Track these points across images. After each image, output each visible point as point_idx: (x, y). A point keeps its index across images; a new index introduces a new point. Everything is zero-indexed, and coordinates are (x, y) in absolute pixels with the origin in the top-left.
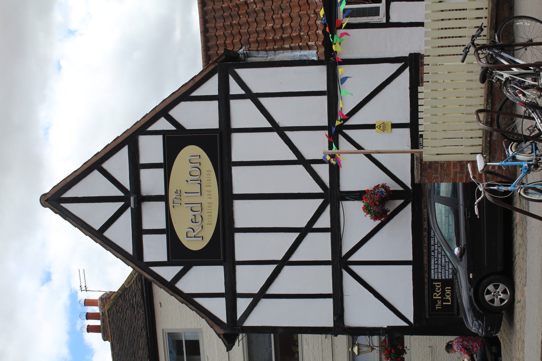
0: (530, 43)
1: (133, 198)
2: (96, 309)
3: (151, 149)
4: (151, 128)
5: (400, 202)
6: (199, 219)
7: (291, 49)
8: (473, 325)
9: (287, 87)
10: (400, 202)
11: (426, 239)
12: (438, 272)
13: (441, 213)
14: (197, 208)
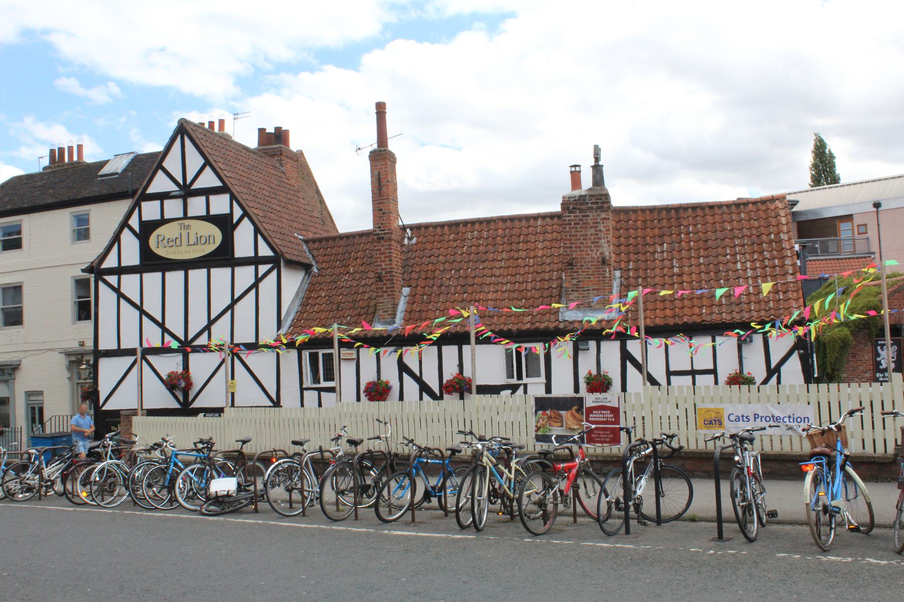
3: (220, 205)
5: (181, 399)
6: (171, 244)
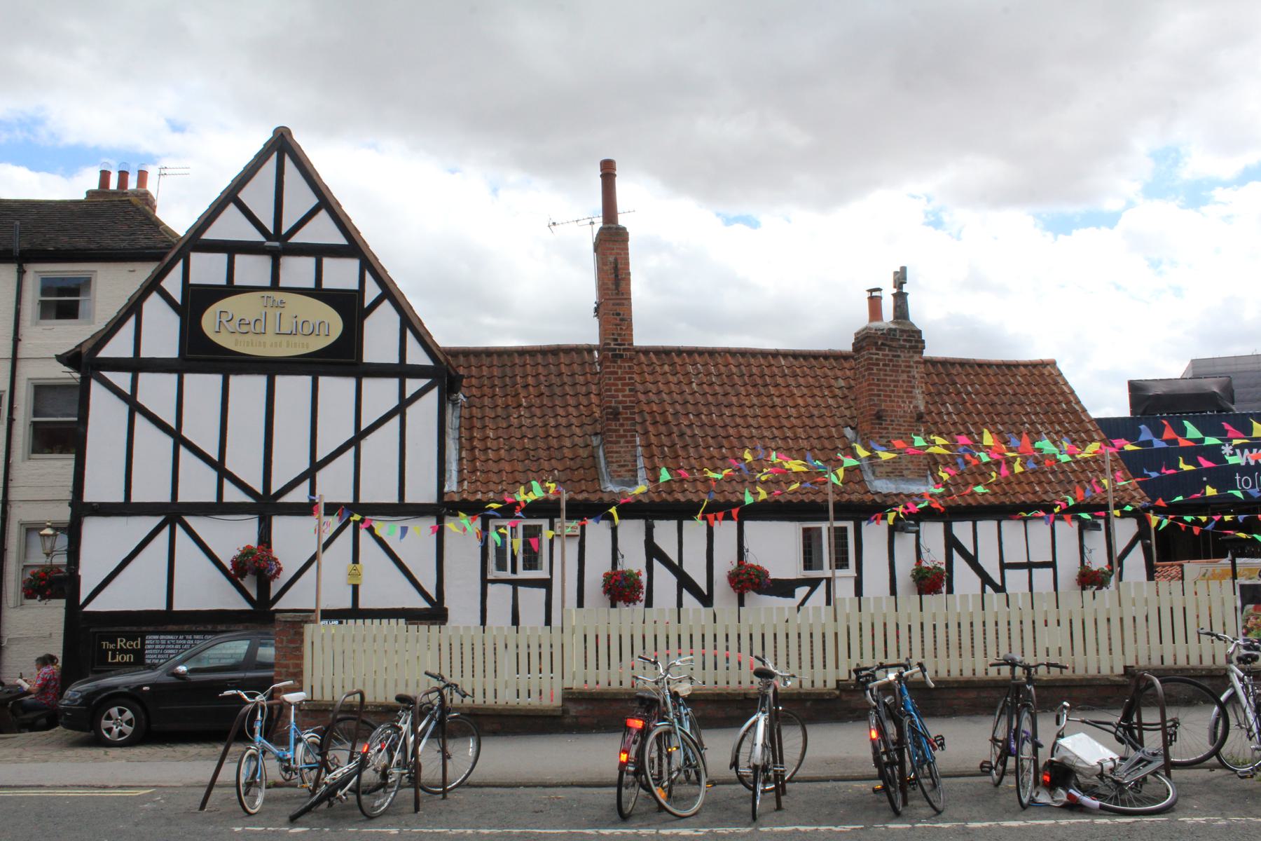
0: (446, 756)
1: (277, 245)
2: (132, 184)
3: (341, 274)
4: (368, 276)
5: (254, 594)
6: (244, 329)
7: (460, 459)
8: (76, 691)
9: (412, 451)
10: (254, 594)
11: (202, 628)
12: (154, 645)
13: (234, 649)
14: (259, 328)
